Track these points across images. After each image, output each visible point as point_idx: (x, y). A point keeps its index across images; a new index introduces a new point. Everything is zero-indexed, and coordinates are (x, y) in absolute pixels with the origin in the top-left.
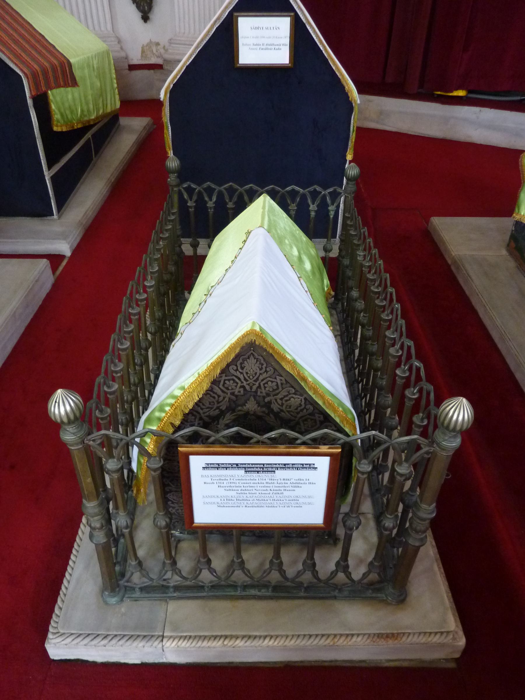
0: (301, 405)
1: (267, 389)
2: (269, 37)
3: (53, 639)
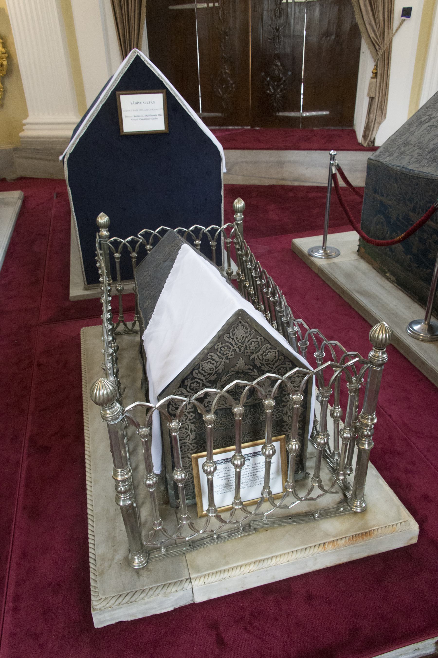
0: (275, 356)
1: (251, 348)
2: (147, 110)
3: (98, 605)
